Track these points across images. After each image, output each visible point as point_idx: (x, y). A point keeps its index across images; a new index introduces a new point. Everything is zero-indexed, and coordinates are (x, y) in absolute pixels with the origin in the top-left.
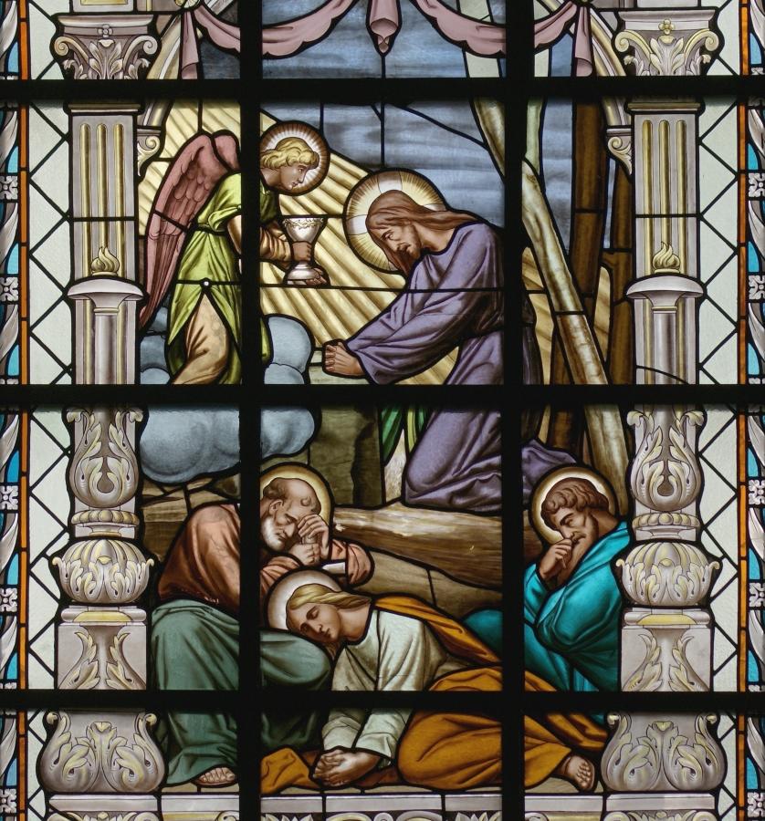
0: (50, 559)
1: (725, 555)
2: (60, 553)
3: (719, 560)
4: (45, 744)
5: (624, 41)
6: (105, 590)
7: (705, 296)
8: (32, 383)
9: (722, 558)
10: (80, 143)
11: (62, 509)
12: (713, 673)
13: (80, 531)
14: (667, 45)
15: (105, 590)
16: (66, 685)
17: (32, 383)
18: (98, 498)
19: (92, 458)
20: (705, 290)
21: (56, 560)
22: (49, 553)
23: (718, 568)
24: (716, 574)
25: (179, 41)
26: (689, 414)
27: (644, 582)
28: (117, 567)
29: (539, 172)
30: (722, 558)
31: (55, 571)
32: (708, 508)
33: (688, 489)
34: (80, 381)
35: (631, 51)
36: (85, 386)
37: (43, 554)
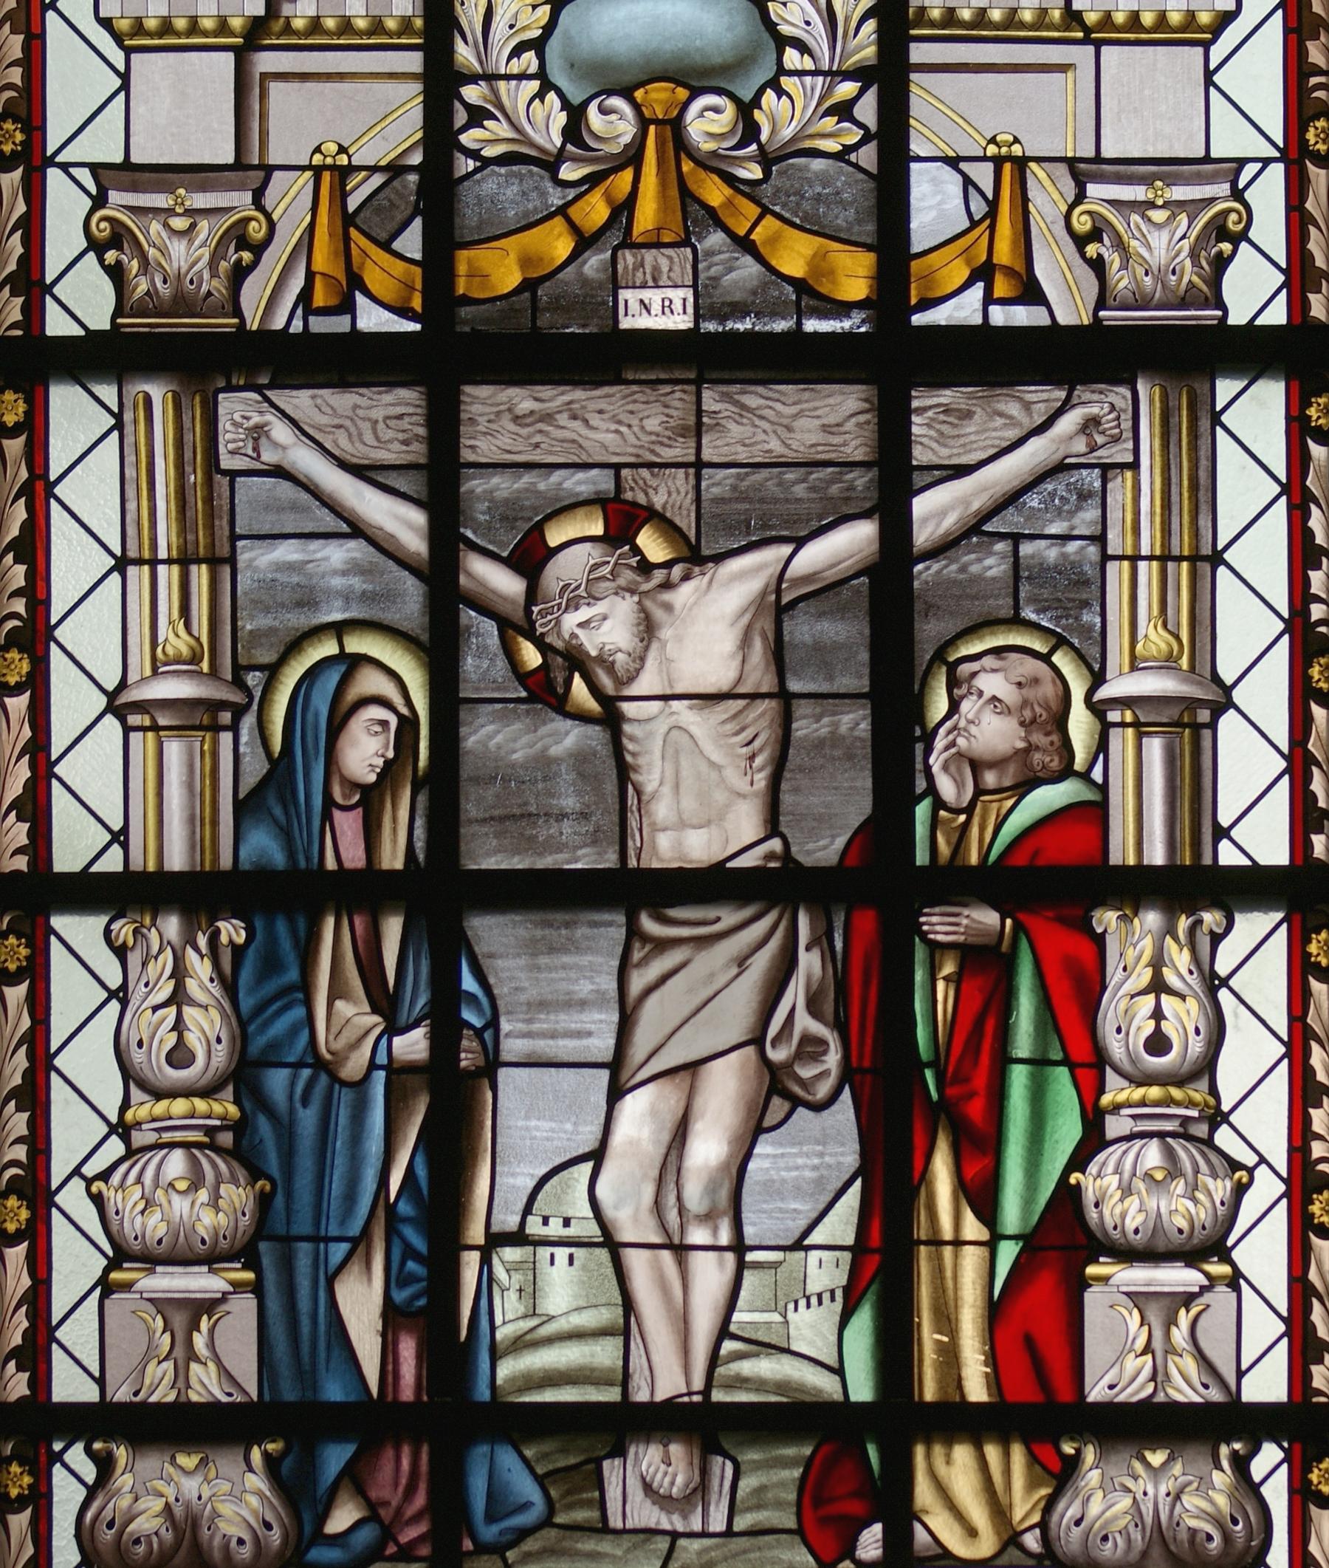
0: (89, 1182)
1: (1262, 1160)
2: (105, 1176)
3: (1250, 1171)
4: (92, 1492)
5: (1085, 218)
6: (1158, 1227)
7: (1230, 704)
8: (1221, 863)
9: (83, 1177)
10: (129, 429)
11: (109, 1094)
12: (1240, 1374)
13: (138, 1139)
14: (1159, 226)
15: (1158, 1227)
16: (122, 1394)
17: (1221, 863)
18: (1174, 1060)
19: (155, 1009)
20: (1229, 697)
21: (97, 1186)
22: (89, 1170)
23: (1245, 1180)
24: (1240, 1190)
25: (308, 218)
26: (221, 924)
27: (139, 1219)
28: (203, 1195)
29: (950, 472)
30: (83, 1177)
31: (98, 1200)
32: (1231, 1081)
33: (1197, 1046)
34: (136, 865)
35: (1095, 235)
36: (144, 874)
37: (77, 1172)
